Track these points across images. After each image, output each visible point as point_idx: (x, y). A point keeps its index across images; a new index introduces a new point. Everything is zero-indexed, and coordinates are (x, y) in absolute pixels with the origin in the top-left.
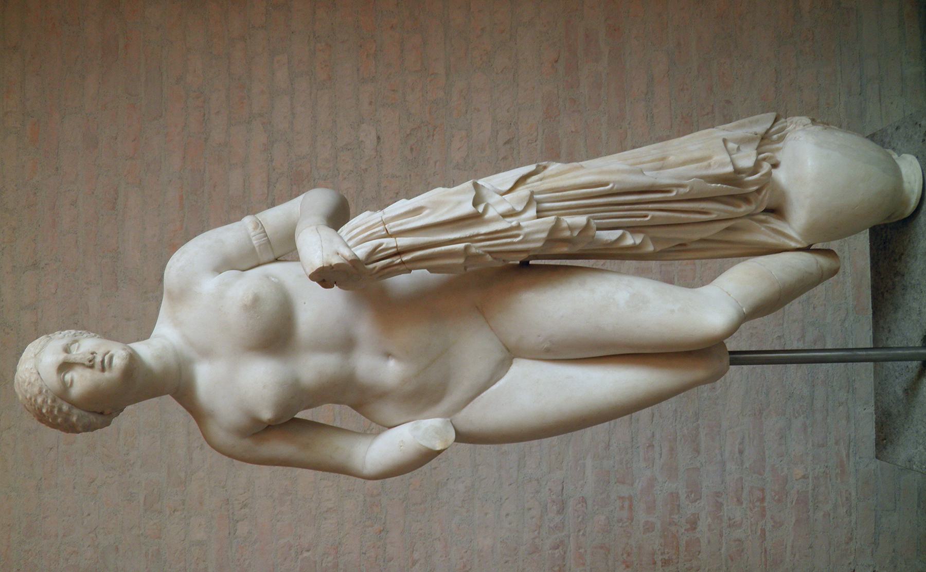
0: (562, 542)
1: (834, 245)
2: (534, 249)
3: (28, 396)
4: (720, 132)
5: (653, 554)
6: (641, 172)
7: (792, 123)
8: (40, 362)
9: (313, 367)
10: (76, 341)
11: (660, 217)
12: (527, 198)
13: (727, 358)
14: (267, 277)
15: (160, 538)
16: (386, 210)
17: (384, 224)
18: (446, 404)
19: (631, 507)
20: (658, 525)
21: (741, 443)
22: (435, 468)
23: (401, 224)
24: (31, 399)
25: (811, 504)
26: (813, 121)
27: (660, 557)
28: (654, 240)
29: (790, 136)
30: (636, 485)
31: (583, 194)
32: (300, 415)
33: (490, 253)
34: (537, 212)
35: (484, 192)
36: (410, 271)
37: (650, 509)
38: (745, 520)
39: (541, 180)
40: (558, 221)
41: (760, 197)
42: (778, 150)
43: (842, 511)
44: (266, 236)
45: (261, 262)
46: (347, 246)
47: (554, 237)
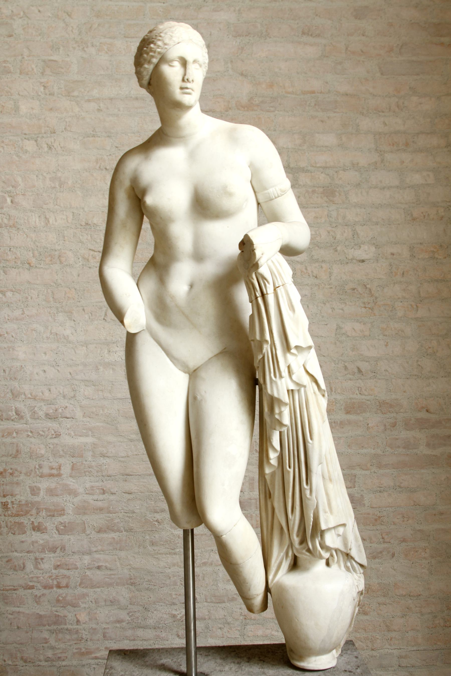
0: (22, 418)
2: (266, 388)
3: (162, 34)
5: (12, 495)
6: (321, 463)
7: (360, 577)
8: (186, 47)
9: (182, 233)
10: (201, 66)
12: (301, 383)
13: (189, 527)
15: (21, 73)
18: (156, 326)
19: (52, 475)
20: (36, 499)
21: (106, 568)
22: (84, 310)
23: (282, 297)
24: (160, 36)
25: (55, 627)
26: (361, 593)
27: (9, 501)
28: (273, 475)
30: (71, 479)
32: (145, 218)
33: (264, 357)
34: (292, 390)
35: (305, 353)
36: (251, 302)
37: (51, 492)
38: (41, 572)
39: (315, 393)
40: (286, 404)
41: (304, 551)
42: (340, 566)
43: (50, 654)
44: (276, 198)
45: (258, 195)
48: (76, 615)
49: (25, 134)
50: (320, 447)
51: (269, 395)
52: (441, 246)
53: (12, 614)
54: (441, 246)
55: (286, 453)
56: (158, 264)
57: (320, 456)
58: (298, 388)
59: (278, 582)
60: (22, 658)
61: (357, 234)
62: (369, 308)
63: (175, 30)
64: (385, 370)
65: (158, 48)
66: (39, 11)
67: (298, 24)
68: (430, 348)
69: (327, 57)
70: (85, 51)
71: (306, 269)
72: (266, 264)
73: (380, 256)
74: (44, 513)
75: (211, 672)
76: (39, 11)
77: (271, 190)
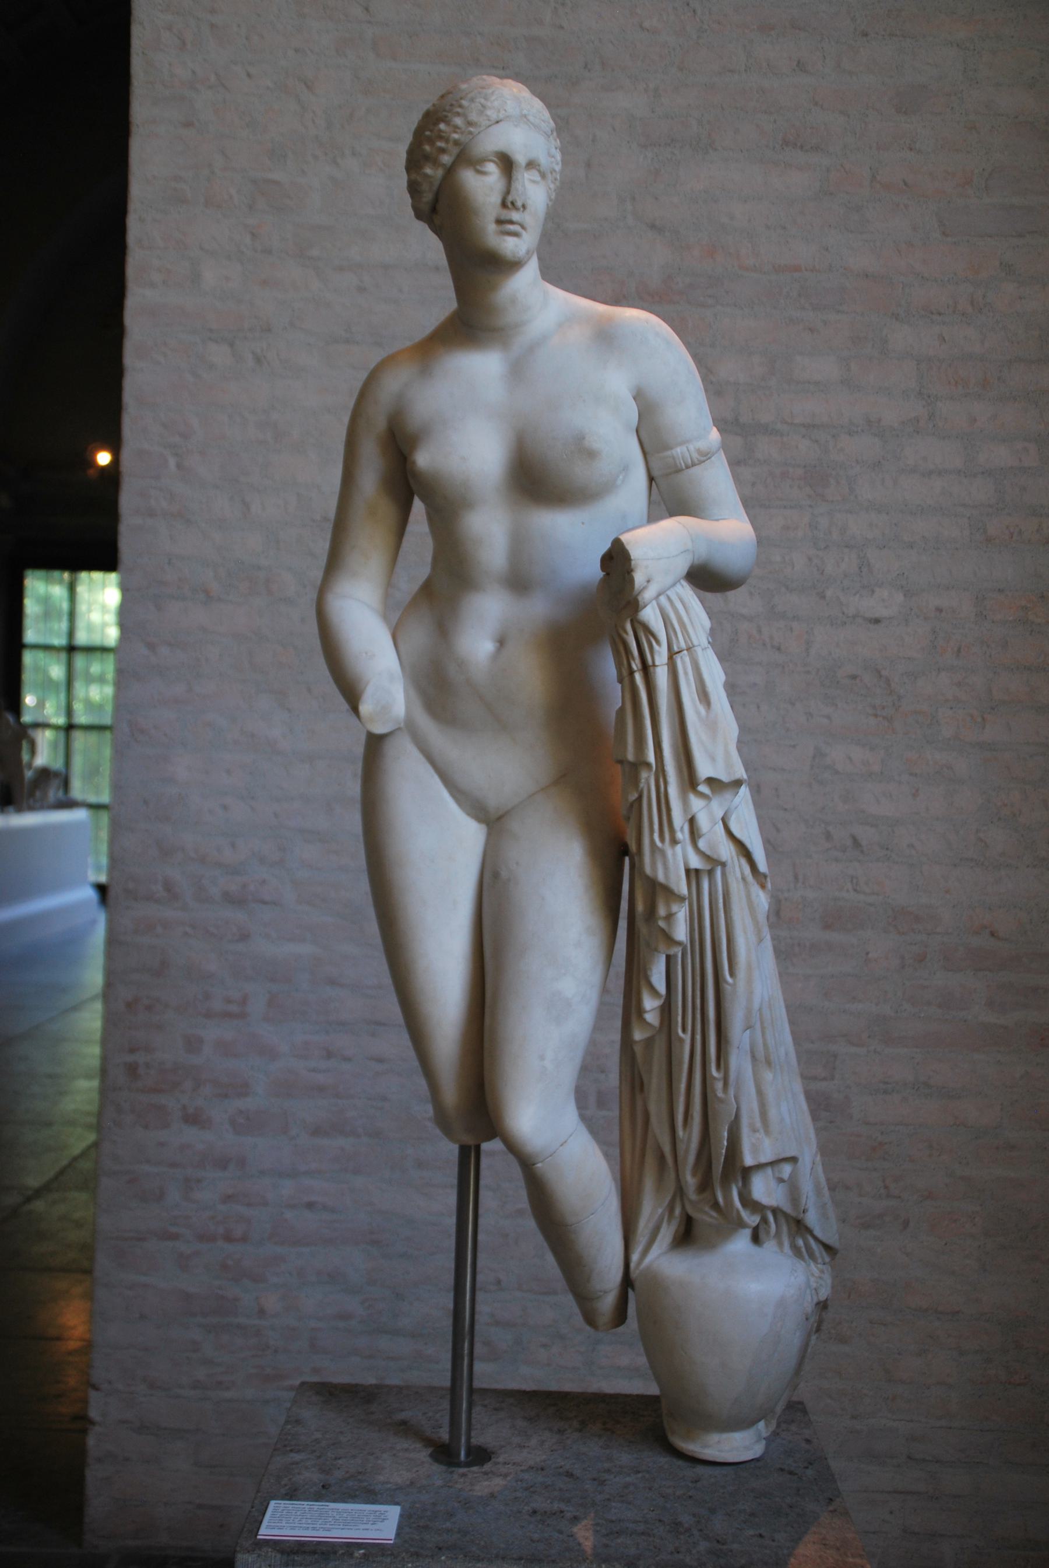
1: (632, 1321)
3: (464, 103)
4: (809, 1155)
6: (749, 1027)
7: (822, 1272)
8: (514, 120)
9: (490, 529)
10: (543, 176)
11: (682, 1053)
12: (715, 857)
13: (469, 1140)
14: (626, 469)
16: (710, 652)
17: (688, 649)
18: (425, 723)
23: (686, 673)
24: (461, 106)
28: (649, 1042)
29: (800, 1265)
31: (719, 938)
32: (418, 506)
33: (640, 798)
34: (697, 871)
35: (728, 795)
36: (620, 680)
39: (744, 879)
40: (681, 899)
41: (707, 1209)
42: (780, 1244)
44: (687, 467)
46: (659, 595)
47: (657, 891)
49: (211, 330)
50: (750, 993)
51: (647, 878)
52: (1043, 597)
54: (1043, 597)
55: (677, 1002)
56: (441, 591)
57: (749, 1011)
58: (708, 867)
62: (884, 718)
63: (493, 93)
64: (908, 846)
65: (455, 132)
66: (249, 75)
67: (775, 122)
68: (1005, 805)
69: (831, 194)
71: (760, 631)
72: (654, 602)
75: (502, 1447)
76: (249, 75)
77: (678, 451)
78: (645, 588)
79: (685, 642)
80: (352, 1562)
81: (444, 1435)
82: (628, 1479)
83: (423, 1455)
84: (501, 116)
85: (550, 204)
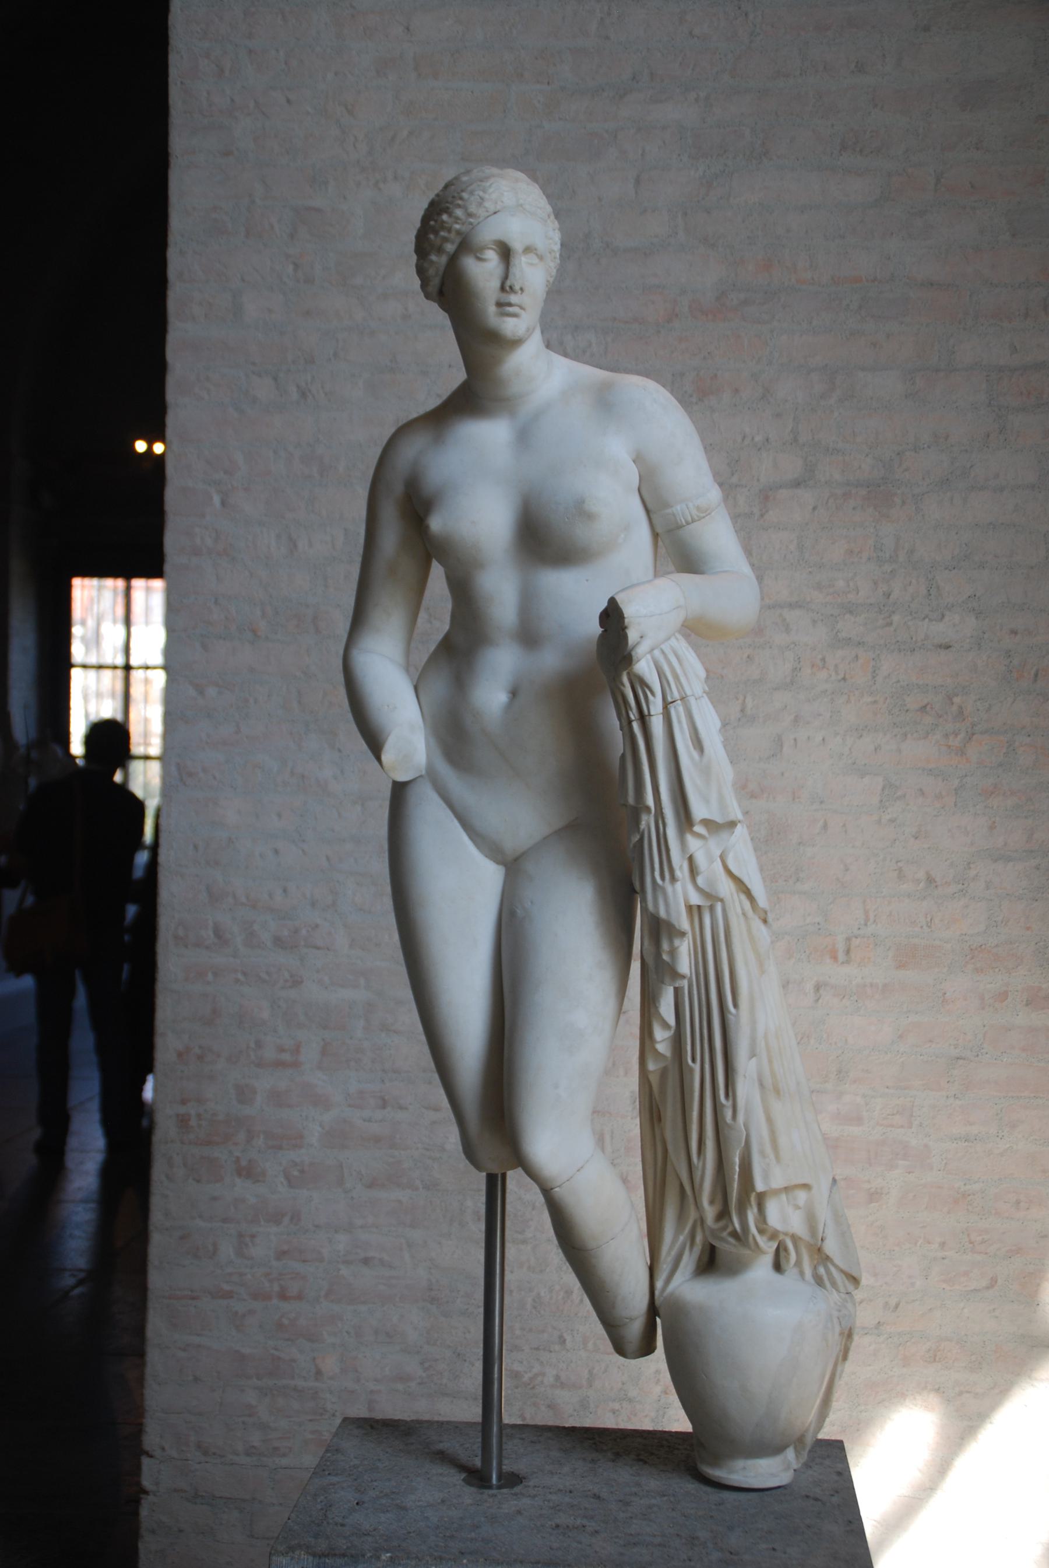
3: (465, 195)
6: (753, 1054)
8: (517, 216)
9: (501, 589)
10: (541, 258)
13: (496, 1170)
17: (682, 699)
18: (444, 769)
23: (680, 722)
24: (461, 198)
27: (193, 1112)
28: (664, 1073)
31: (722, 971)
33: (641, 839)
34: (699, 907)
35: (724, 835)
39: (744, 914)
44: (688, 523)
45: (653, 516)
48: (314, 1359)
50: (753, 1022)
51: (652, 914)
53: (184, 1350)
59: (672, 1294)
60: (199, 1446)
61: (938, 588)
63: (490, 186)
66: (288, 101)
67: (833, 125)
70: (380, 189)
72: (649, 656)
73: (986, 636)
74: (260, 1142)
76: (288, 101)
77: (678, 508)
78: (638, 643)
79: (679, 692)
80: (380, 1565)
81: (478, 1462)
82: (653, 1501)
83: (457, 1478)
84: (498, 208)
85: (551, 280)
